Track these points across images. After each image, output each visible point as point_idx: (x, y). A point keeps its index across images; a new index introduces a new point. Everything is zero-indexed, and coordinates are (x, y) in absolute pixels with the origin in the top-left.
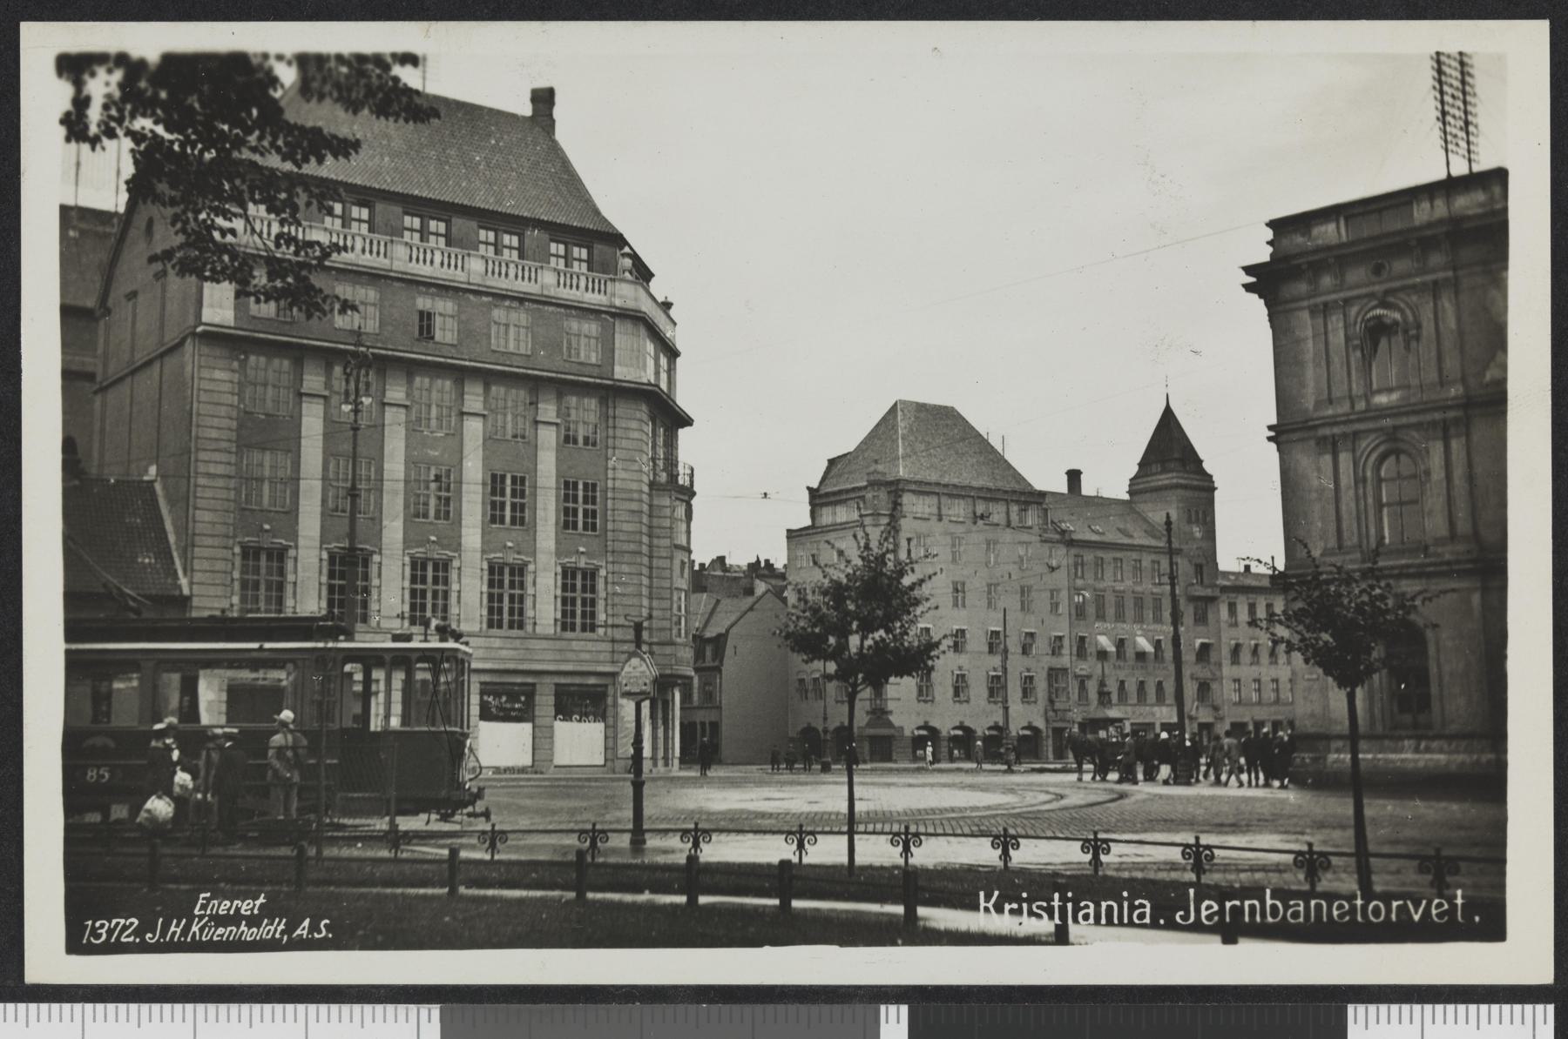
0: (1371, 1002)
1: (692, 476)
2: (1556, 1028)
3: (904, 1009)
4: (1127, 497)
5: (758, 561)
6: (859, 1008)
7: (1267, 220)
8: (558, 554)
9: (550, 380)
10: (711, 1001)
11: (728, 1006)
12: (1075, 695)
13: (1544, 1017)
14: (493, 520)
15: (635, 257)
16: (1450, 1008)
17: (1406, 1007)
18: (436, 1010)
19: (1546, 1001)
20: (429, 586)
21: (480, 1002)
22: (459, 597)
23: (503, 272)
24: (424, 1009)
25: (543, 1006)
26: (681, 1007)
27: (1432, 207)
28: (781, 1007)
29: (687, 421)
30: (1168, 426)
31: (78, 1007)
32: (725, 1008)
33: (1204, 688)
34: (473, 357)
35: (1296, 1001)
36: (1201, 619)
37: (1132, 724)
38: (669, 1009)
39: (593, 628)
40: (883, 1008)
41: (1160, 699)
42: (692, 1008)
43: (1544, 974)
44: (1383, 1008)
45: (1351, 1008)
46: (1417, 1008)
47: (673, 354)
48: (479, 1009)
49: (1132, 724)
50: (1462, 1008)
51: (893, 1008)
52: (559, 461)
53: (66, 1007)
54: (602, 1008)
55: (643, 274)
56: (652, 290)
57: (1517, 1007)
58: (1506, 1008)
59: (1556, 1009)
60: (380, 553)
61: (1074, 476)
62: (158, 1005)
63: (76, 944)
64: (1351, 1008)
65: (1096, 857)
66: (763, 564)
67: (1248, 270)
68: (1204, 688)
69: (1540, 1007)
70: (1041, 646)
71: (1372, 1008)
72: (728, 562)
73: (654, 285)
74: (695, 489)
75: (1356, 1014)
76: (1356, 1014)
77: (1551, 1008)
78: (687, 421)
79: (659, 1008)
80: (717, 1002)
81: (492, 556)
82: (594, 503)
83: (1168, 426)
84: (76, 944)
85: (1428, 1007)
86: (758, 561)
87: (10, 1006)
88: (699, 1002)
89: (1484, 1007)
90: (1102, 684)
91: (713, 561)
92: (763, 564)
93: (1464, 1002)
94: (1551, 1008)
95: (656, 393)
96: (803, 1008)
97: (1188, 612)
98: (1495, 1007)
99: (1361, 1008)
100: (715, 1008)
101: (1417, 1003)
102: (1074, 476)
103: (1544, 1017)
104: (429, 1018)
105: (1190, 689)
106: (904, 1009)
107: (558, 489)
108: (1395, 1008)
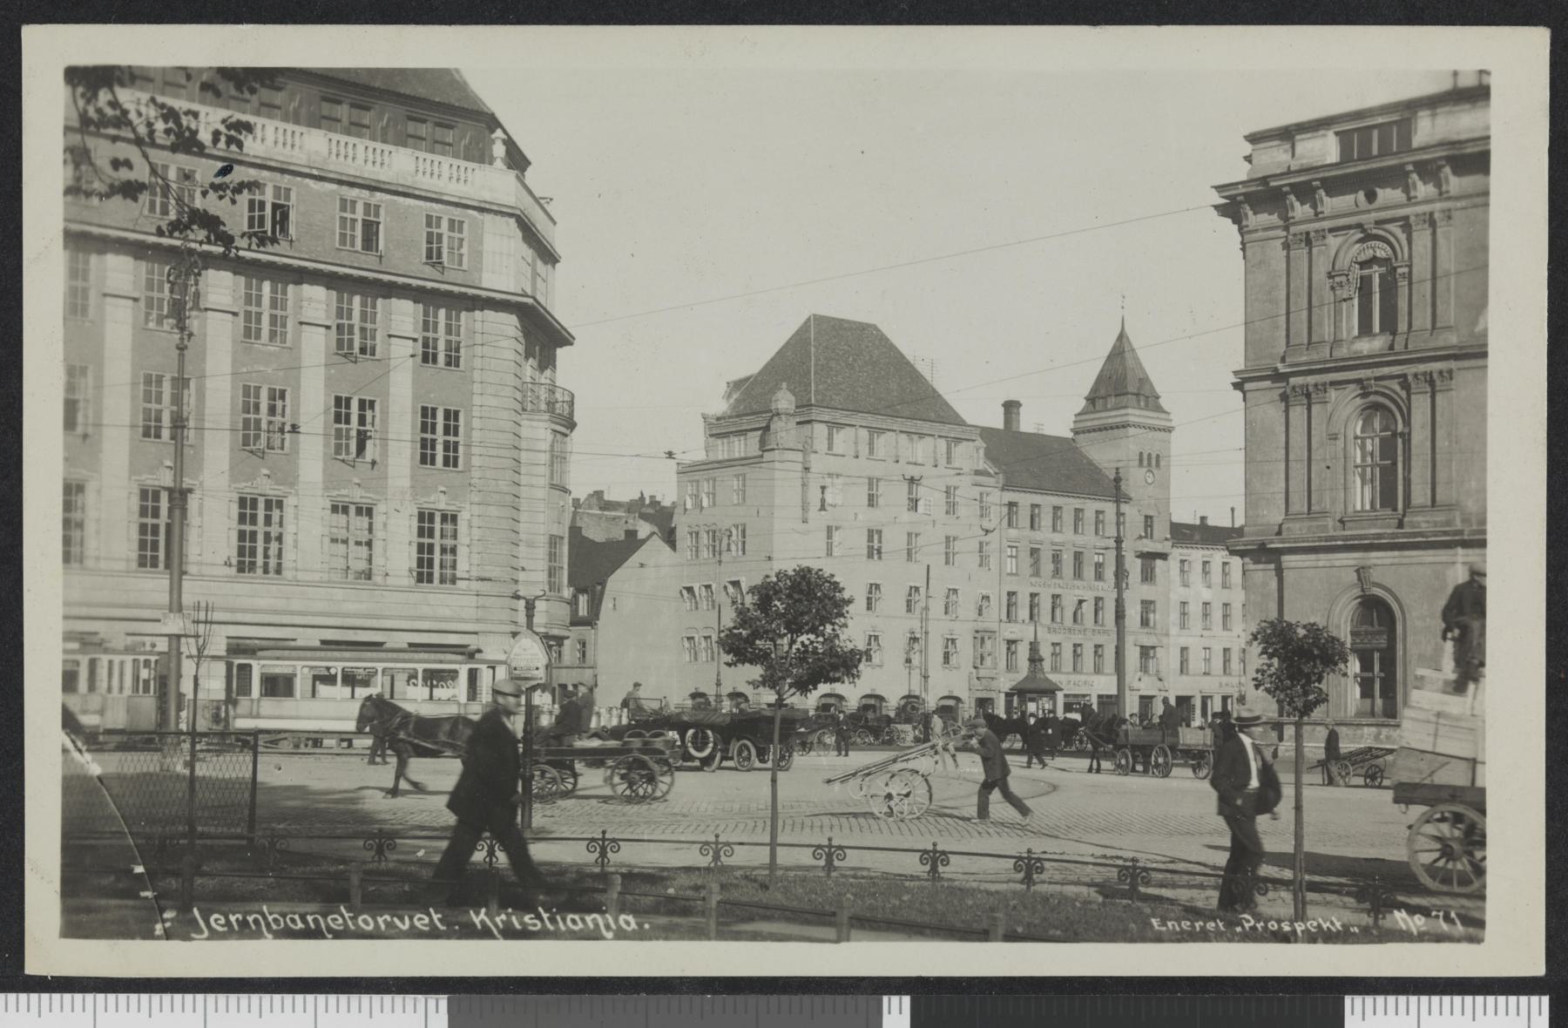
0: (1368, 993)
1: (572, 403)
2: (1551, 1019)
3: (907, 1000)
4: (1070, 435)
5: (642, 498)
6: (862, 999)
7: (1247, 133)
8: (133, 470)
9: (407, 287)
10: (715, 992)
11: (732, 997)
12: (1002, 664)
13: (1540, 1006)
14: (146, 434)
15: (510, 144)
16: (1446, 999)
17: (1402, 999)
18: (443, 1000)
19: (1541, 993)
20: (260, 528)
21: (487, 992)
22: (296, 541)
23: (351, 155)
24: (432, 999)
25: (548, 997)
26: (685, 998)
27: (1433, 125)
28: (785, 998)
29: (564, 339)
30: (1120, 351)
31: (89, 997)
32: (729, 999)
33: (1146, 652)
34: (313, 257)
35: (1293, 993)
36: (1148, 576)
37: (1066, 696)
38: (674, 999)
39: (454, 580)
40: (885, 999)
41: (1098, 670)
42: (697, 998)
43: (1536, 966)
44: (1380, 999)
45: (1348, 999)
46: (1413, 999)
47: (548, 256)
48: (487, 999)
49: (1066, 696)
50: (1457, 999)
51: (895, 999)
52: (417, 382)
53: (78, 997)
54: (608, 999)
55: (517, 160)
56: (527, 181)
57: (1513, 999)
58: (1502, 999)
59: (1551, 1000)
60: (297, 495)
61: (1011, 407)
62: (14, 995)
63: (77, 924)
64: (1348, 999)
65: (934, 869)
66: (647, 502)
67: (1220, 188)
68: (1146, 652)
69: (1535, 999)
70: (966, 608)
71: (1369, 999)
72: (606, 497)
73: (529, 172)
74: (575, 419)
75: (1353, 1005)
76: (1353, 1005)
77: (1546, 999)
78: (564, 339)
79: (663, 999)
80: (722, 993)
81: (335, 493)
82: (456, 434)
83: (1120, 351)
84: (77, 924)
85: (1424, 999)
86: (642, 498)
87: (12, 996)
88: (704, 993)
89: (1480, 999)
90: (1034, 647)
91: (591, 496)
92: (647, 502)
93: (1459, 994)
94: (1546, 999)
95: (533, 307)
96: (806, 998)
97: (1134, 566)
98: (1491, 999)
99: (1358, 999)
100: (719, 998)
101: (1414, 994)
102: (1011, 407)
103: (1540, 1006)
104: (438, 1006)
105: (1132, 656)
106: (907, 1000)
107: (134, 384)
108: (1391, 999)
